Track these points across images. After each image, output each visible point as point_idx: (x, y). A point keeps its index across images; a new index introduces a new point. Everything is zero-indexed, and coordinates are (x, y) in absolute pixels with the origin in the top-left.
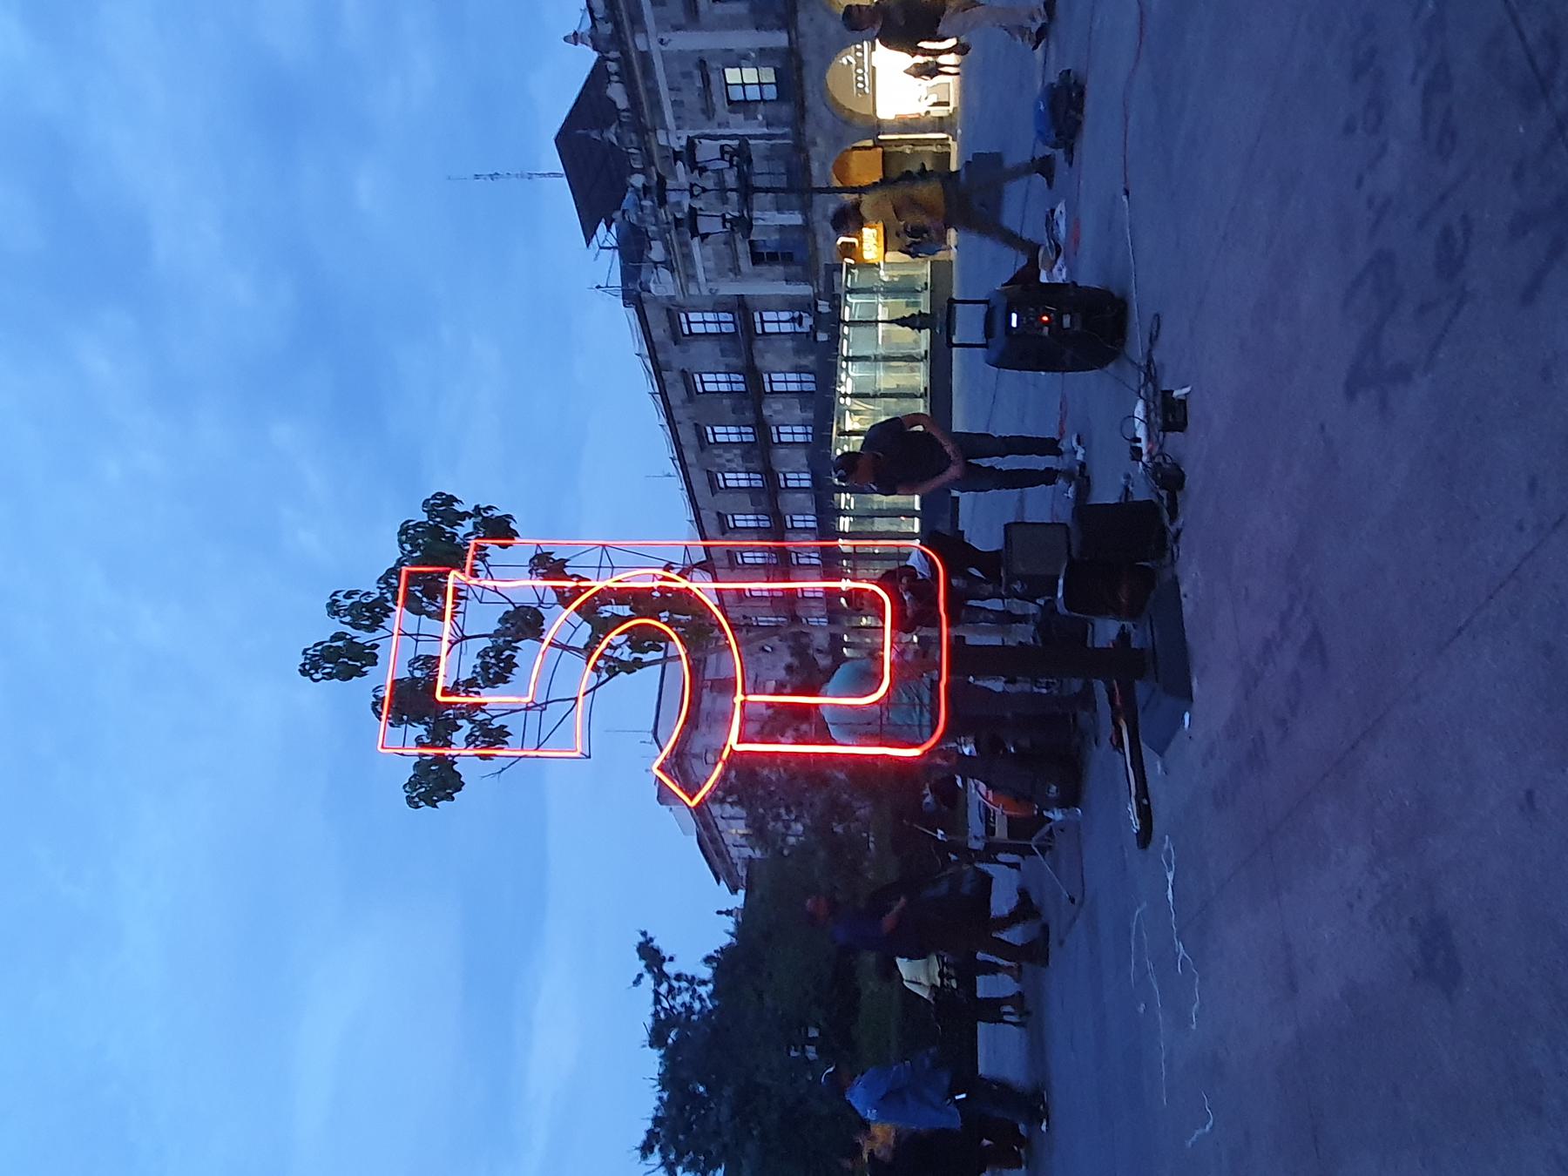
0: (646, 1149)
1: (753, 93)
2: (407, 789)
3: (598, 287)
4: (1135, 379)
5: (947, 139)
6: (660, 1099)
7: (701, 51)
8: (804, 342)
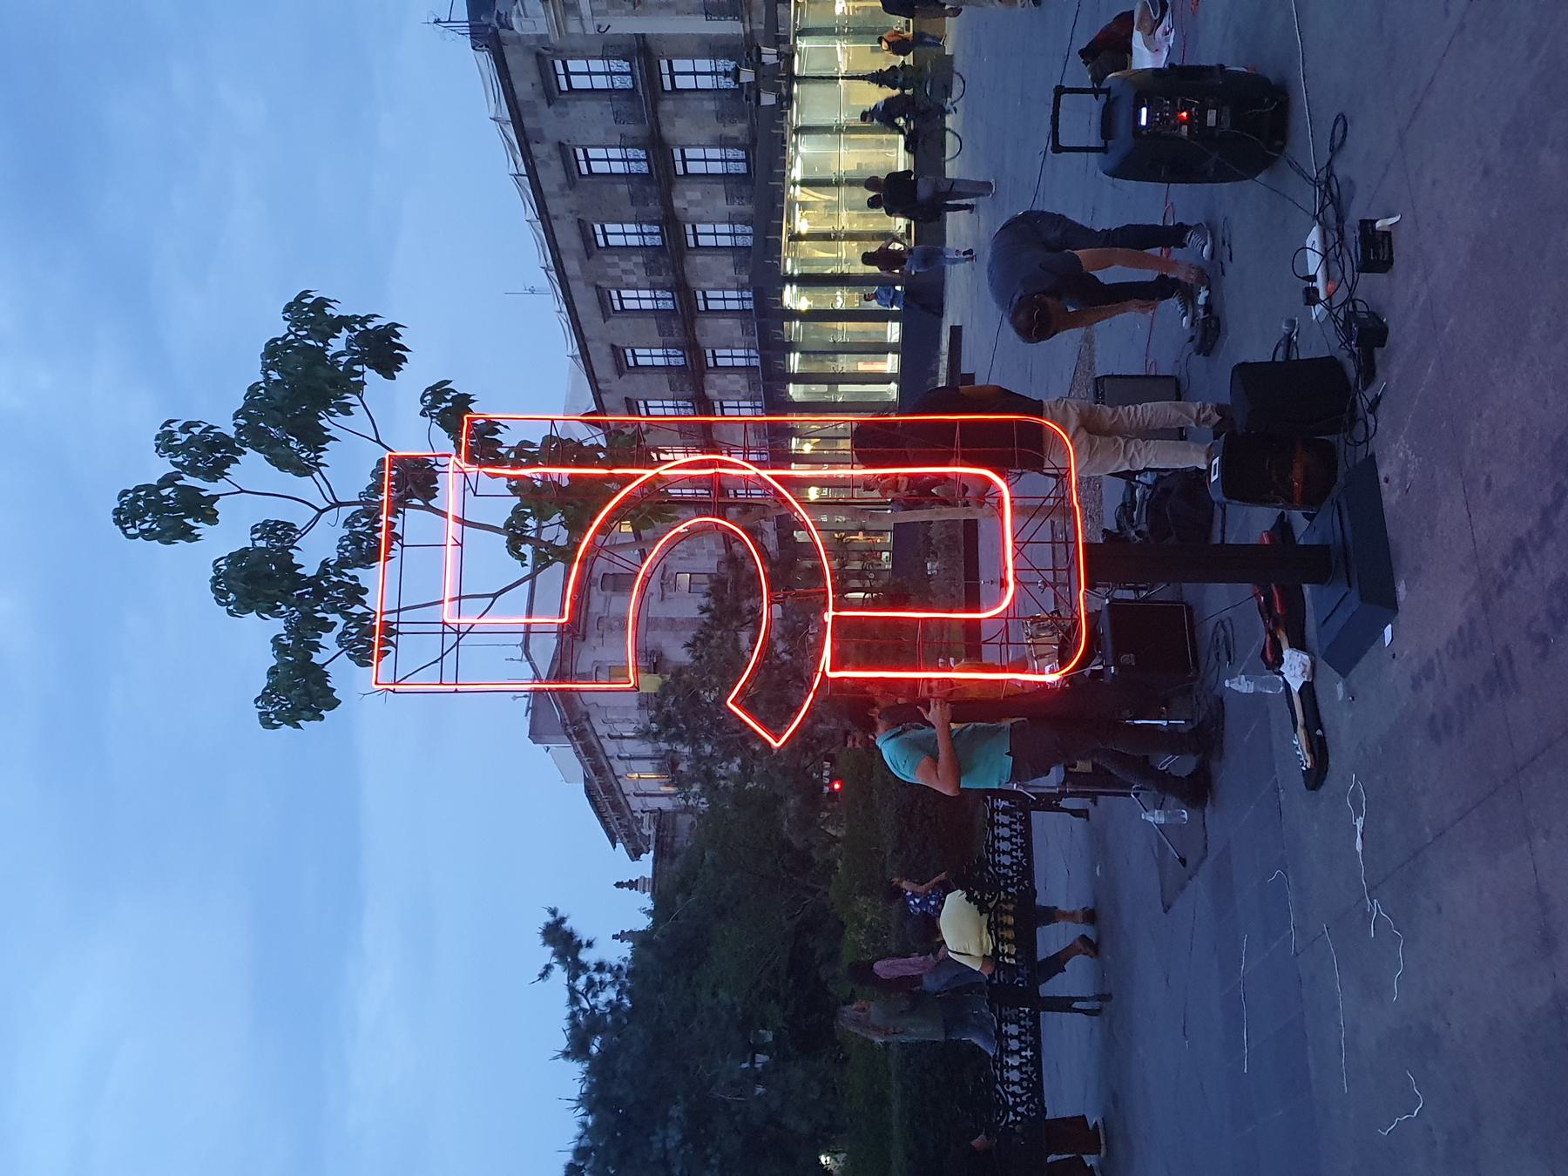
3: (437, 21)
4: (1310, 197)
6: (584, 1124)
8: (737, 101)
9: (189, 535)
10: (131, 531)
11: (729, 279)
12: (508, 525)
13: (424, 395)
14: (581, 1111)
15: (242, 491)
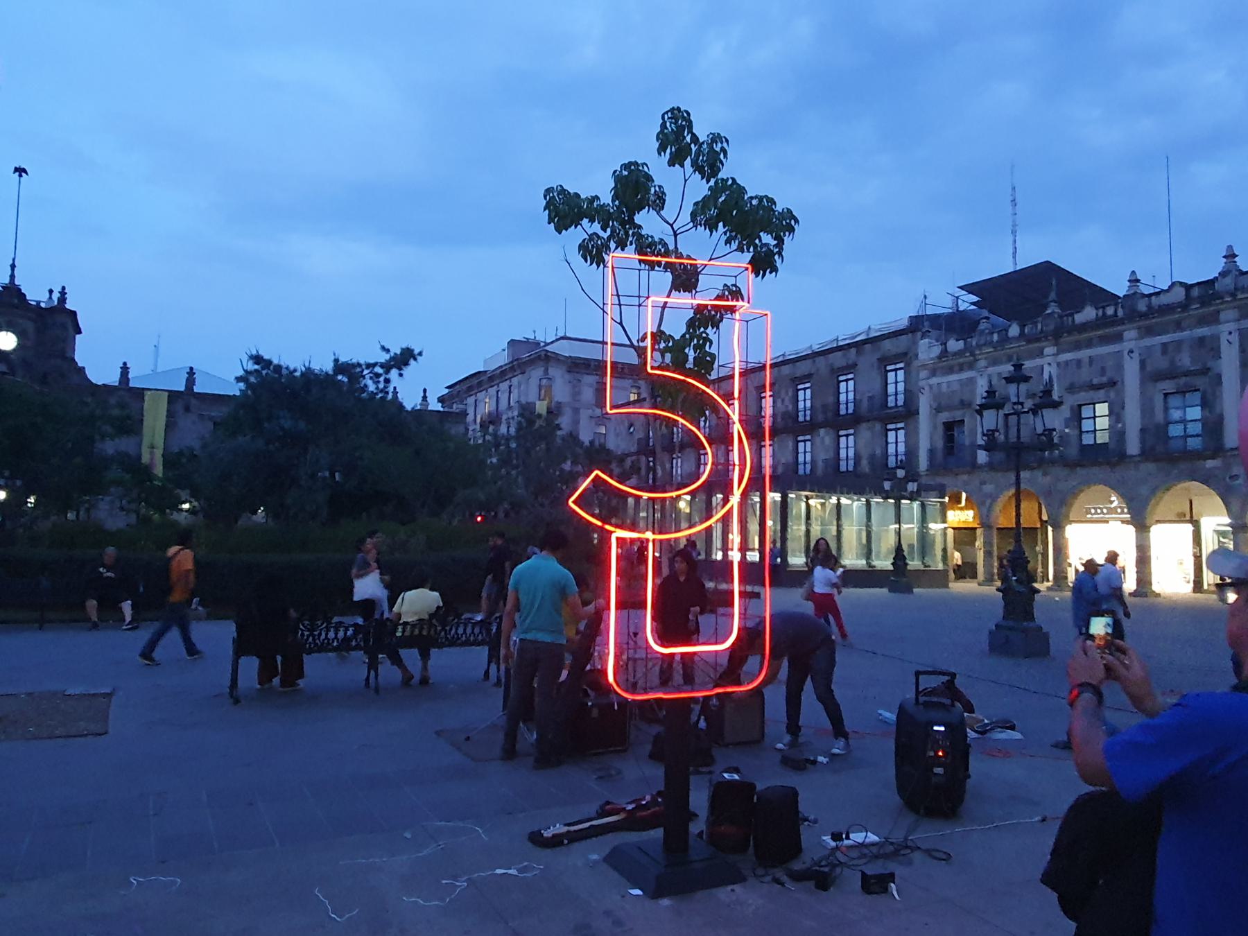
0: (257, 359)
1: (1087, 425)
2: (559, 188)
3: (925, 297)
4: (898, 837)
5: (1048, 581)
6: (295, 370)
7: (1123, 382)
9: (662, 149)
14: (303, 369)
15: (686, 181)
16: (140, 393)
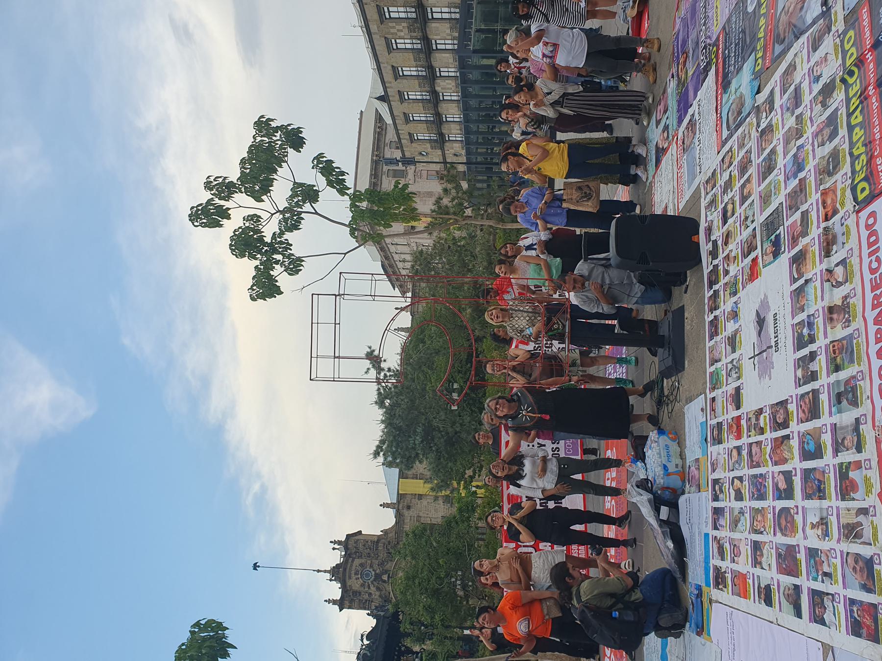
0: (376, 454)
10: (196, 224)
11: (448, 35)
12: (350, 224)
13: (313, 160)
16: (401, 497)
